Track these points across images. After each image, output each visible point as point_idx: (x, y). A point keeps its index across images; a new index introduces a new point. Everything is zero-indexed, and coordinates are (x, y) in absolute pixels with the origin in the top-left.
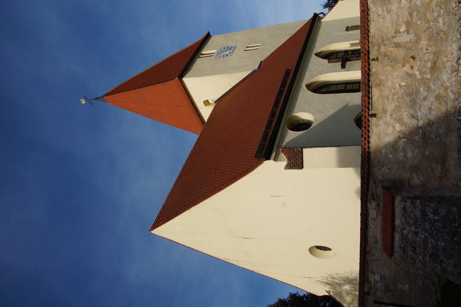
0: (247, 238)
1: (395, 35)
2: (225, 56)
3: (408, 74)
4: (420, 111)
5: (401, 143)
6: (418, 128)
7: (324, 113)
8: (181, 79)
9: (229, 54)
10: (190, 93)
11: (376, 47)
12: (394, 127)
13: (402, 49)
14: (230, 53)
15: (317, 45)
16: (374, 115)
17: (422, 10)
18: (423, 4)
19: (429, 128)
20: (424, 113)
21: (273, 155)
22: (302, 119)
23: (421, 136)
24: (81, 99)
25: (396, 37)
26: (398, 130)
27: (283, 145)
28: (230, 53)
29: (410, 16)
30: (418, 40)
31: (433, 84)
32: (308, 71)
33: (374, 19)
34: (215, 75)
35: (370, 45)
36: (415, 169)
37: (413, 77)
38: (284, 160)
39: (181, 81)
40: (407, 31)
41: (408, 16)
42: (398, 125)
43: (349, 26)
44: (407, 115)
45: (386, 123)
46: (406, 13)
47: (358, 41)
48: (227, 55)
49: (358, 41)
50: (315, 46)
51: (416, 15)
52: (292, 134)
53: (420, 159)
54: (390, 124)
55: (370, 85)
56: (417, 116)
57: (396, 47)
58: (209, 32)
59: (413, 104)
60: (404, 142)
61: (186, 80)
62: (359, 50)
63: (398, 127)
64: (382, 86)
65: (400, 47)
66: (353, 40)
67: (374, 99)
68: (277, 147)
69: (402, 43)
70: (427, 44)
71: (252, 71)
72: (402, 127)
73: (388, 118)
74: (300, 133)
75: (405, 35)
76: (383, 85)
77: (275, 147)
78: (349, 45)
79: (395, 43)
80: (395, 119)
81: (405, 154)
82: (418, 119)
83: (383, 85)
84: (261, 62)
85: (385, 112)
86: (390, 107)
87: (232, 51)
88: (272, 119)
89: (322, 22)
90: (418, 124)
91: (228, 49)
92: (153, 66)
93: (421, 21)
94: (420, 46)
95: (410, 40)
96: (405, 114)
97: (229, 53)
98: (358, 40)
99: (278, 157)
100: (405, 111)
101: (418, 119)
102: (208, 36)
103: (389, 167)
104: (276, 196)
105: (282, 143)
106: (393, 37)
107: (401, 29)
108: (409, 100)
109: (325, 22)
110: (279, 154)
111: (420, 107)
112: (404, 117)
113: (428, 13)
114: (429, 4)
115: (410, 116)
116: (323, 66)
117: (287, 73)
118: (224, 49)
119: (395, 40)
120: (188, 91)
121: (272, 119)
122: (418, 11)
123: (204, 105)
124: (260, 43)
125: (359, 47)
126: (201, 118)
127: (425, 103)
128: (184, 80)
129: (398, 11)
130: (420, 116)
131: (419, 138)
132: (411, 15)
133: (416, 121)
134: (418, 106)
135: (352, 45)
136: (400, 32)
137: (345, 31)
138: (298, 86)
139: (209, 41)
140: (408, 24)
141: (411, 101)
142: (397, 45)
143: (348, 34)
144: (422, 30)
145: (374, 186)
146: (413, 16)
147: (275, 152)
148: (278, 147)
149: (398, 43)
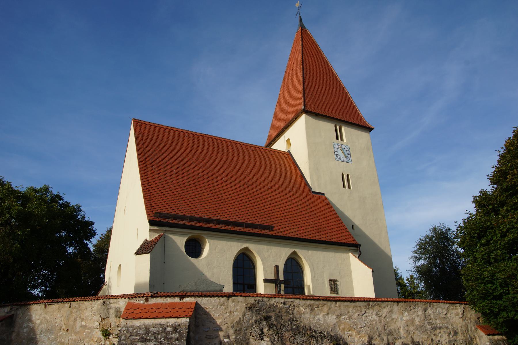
0: (125, 210)
1: (81, 318)
2: (336, 153)
3: (61, 327)
4: (43, 336)
5: (31, 325)
6: (35, 334)
7: (207, 267)
8: (304, 112)
9: (339, 157)
10: (294, 123)
11: (77, 306)
12: (38, 319)
13: (73, 323)
14: (340, 158)
15: (310, 252)
16: (46, 306)
17: (90, 335)
18: (93, 336)
19: (35, 342)
20: (42, 338)
21: (155, 228)
22: (205, 248)
23: (32, 337)
24: (299, 2)
25: (80, 319)
26: (37, 322)
27: (169, 235)
28: (340, 158)
29: (89, 328)
30: (76, 333)
31: (54, 343)
32: (269, 247)
33: (92, 304)
34: (308, 148)
35: (79, 302)
36: (18, 334)
37: (59, 330)
38: (150, 238)
39: (302, 113)
40: (81, 326)
41: (89, 327)
42: (39, 322)
43: (339, 281)
44: (43, 327)
45: (41, 315)
46: (91, 326)
47: (312, 293)
48: (337, 155)
49: (312, 293)
50: (308, 250)
51: (88, 332)
52: (181, 241)
53: (22, 337)
54: (40, 317)
55: (59, 303)
56: (42, 334)
57: (75, 319)
58: (373, 129)
59: (48, 331)
60: (31, 326)
61: (303, 117)
62: (304, 294)
63: (38, 322)
64: (58, 310)
65: (74, 322)
66: (313, 288)
67: (53, 305)
68: (165, 230)
69: (76, 323)
70: (73, 339)
71: (311, 186)
72: (38, 325)
73: (43, 316)
74: (183, 248)
75: (80, 325)
76: (59, 311)
77: (164, 228)
78: (309, 284)
79: (76, 319)
80: (42, 320)
81: (25, 327)
82: (40, 334)
83: (59, 311)
84: (323, 194)
85: (46, 313)
86: (47, 316)
87: (344, 160)
88: (203, 221)
89: (349, 253)
90: (37, 335)
91: (346, 154)
92: (336, 75)
93: (85, 335)
94: (73, 334)
95: (77, 328)
96: (43, 326)
97: (340, 157)
98: (313, 292)
99: (154, 232)
100: (45, 326)
101: (40, 334)
102: (369, 129)
103: (22, 318)
104: (137, 233)
105: (171, 234)
106: (80, 317)
107: (84, 322)
108: (49, 329)
109: (348, 258)
110: (158, 233)
111: (45, 335)
112: (42, 326)
113: (88, 339)
114: (93, 340)
115: (42, 329)
116: (274, 261)
117: (270, 228)
118: (348, 150)
119: (78, 318)
120: (295, 121)
121: (203, 221)
122: (90, 333)
123: (287, 140)
124: (352, 188)
125: (306, 294)
126: (278, 138)
127: (46, 338)
128: (302, 116)
129: (93, 320)
130: (41, 336)
131: (31, 336)
132: (89, 328)
133: (39, 333)
134: (46, 334)
135: (309, 287)
136: (82, 321)
137: (329, 279)
138: (247, 240)
139: (361, 131)
140: (85, 327)
141: (49, 330)
142: (75, 320)
143: (324, 283)
144: (80, 335)
145: (15, 309)
146: (89, 330)
147: (159, 229)
148: (165, 231)
149: (76, 321)
